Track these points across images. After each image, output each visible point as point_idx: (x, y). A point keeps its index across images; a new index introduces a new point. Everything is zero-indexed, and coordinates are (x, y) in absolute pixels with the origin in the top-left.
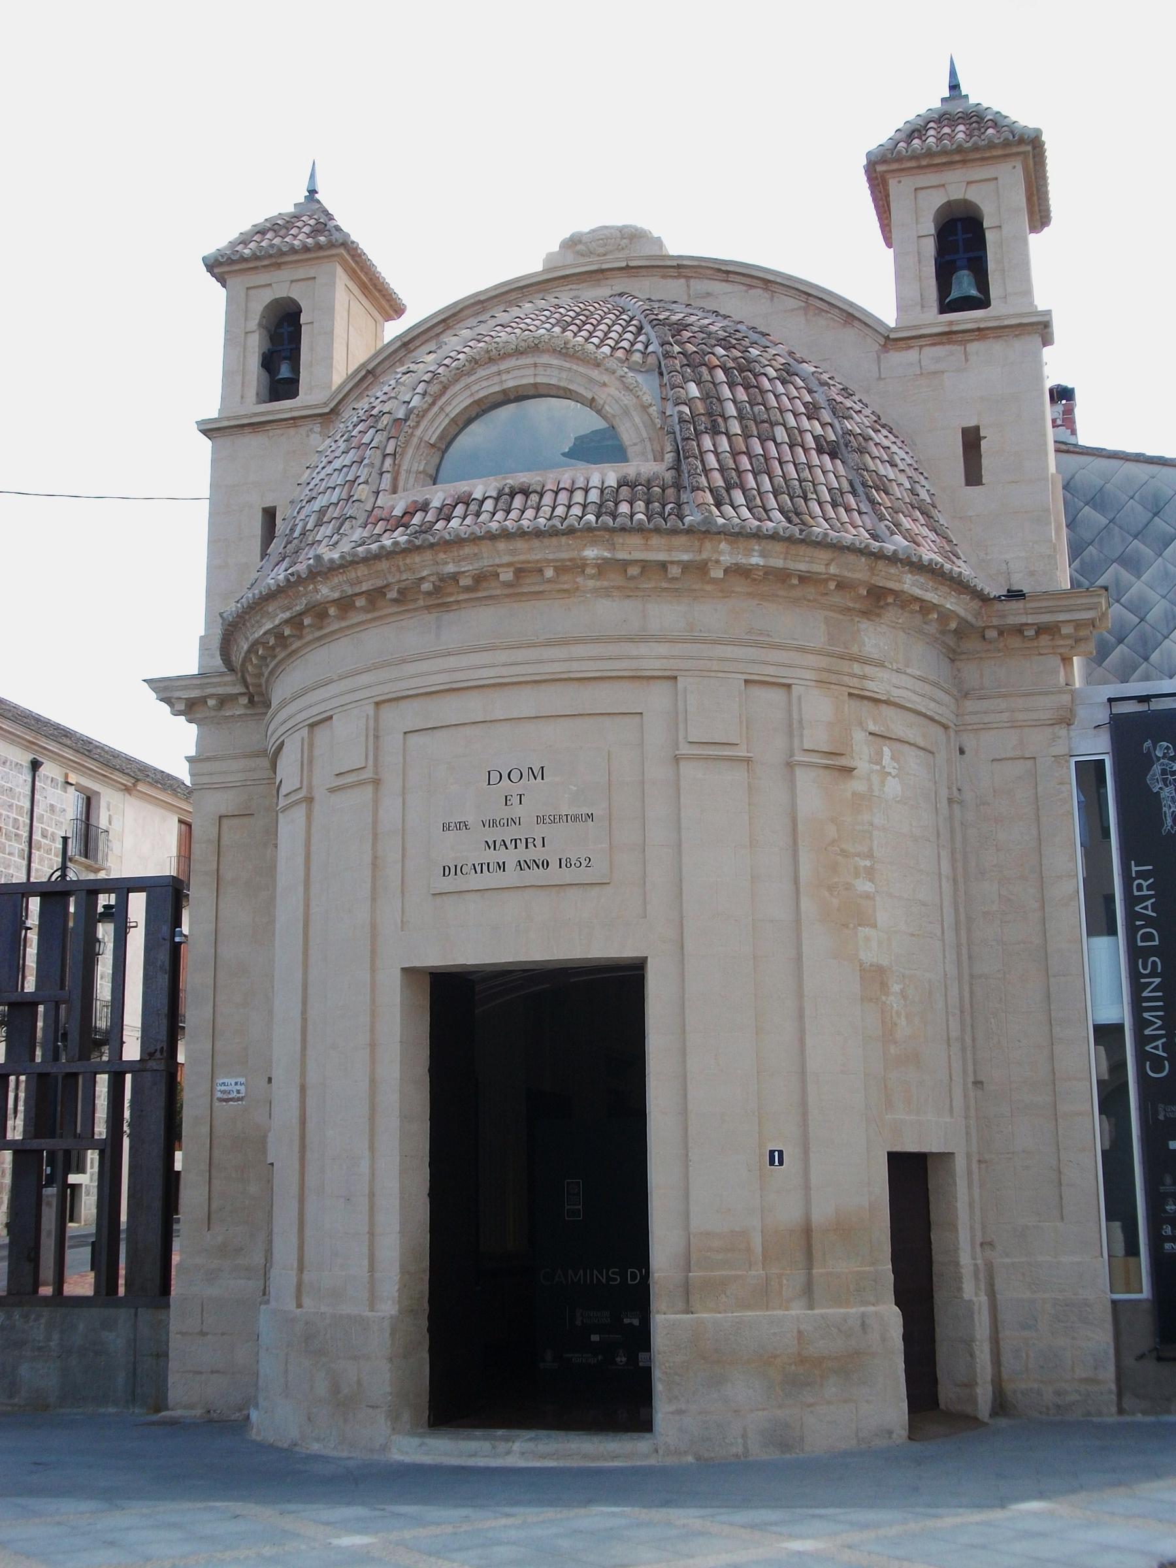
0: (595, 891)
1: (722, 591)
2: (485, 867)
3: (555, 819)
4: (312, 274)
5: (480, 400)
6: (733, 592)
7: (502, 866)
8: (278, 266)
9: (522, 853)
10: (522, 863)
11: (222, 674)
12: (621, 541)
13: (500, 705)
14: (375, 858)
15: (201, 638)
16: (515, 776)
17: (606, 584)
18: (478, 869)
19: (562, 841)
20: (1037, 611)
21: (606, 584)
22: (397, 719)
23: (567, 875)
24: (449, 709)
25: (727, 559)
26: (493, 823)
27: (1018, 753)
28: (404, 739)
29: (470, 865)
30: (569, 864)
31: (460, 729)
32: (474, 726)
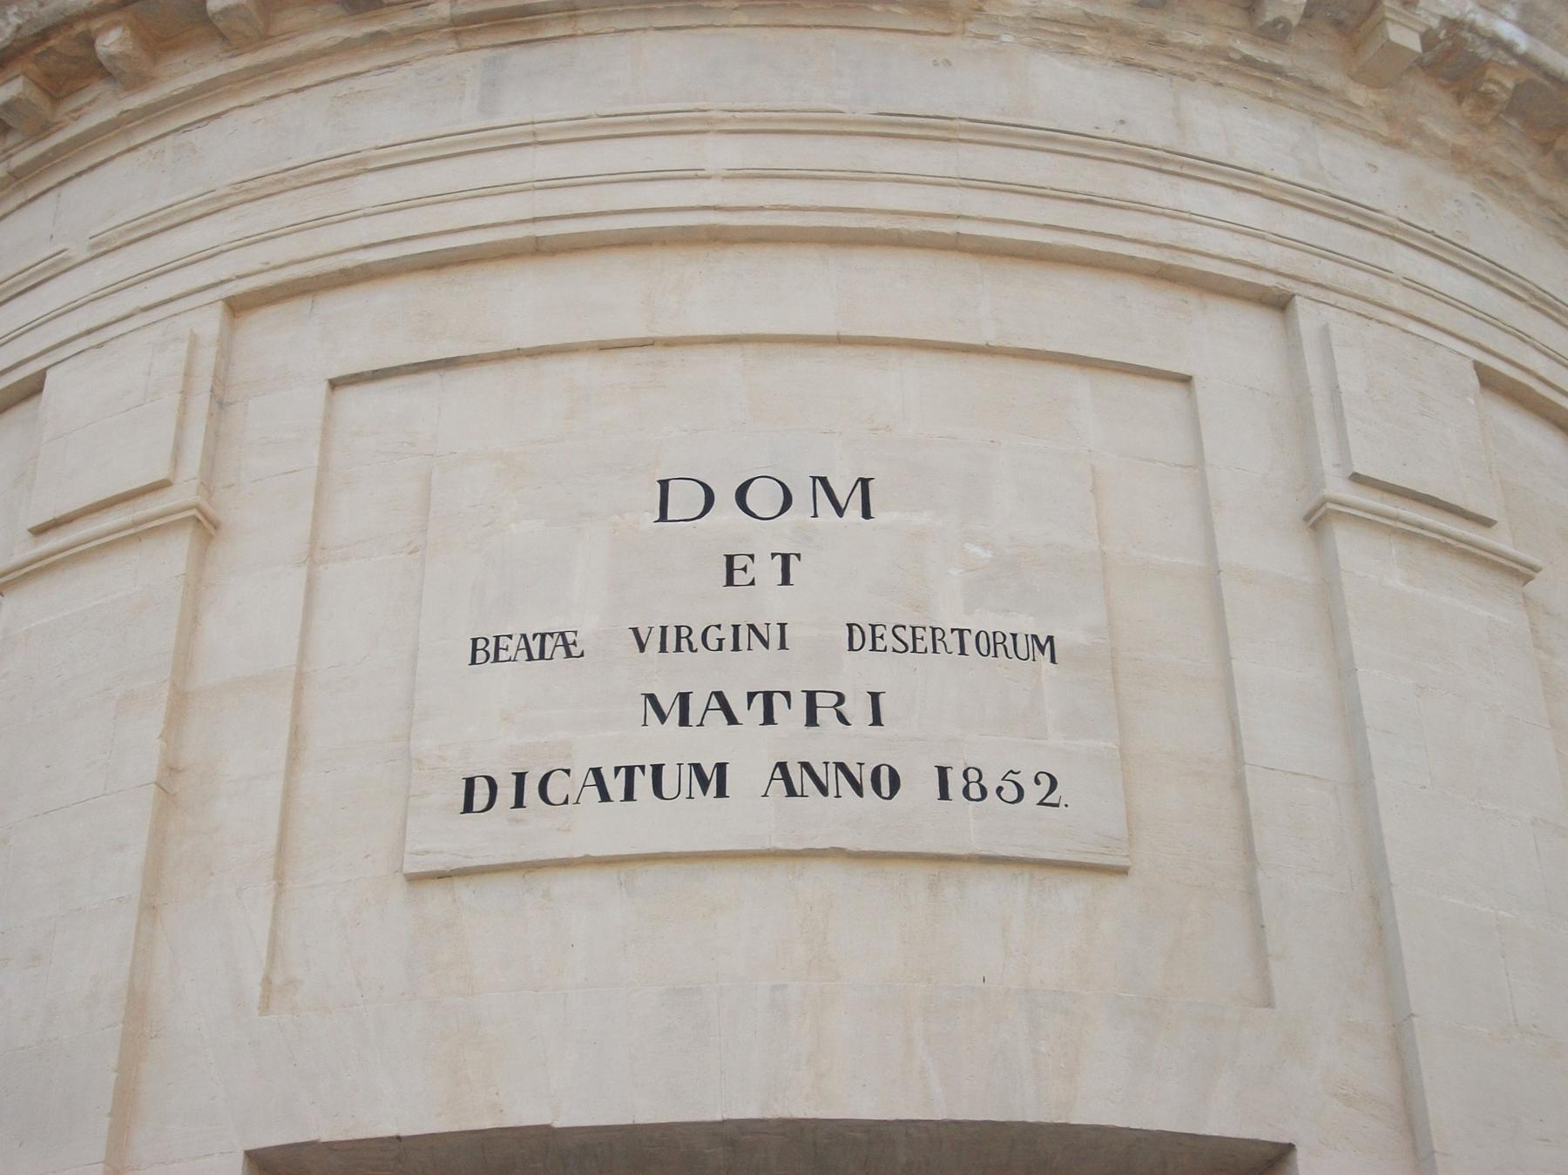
1: (1389, 118)
2: (643, 782)
6: (1418, 132)
7: (713, 780)
9: (790, 737)
10: (795, 772)
13: (705, 294)
14: (171, 769)
16: (763, 498)
18: (616, 786)
23: (967, 825)
24: (520, 304)
26: (677, 639)
28: (329, 401)
29: (580, 772)
30: (975, 789)
31: (551, 365)
32: (603, 358)
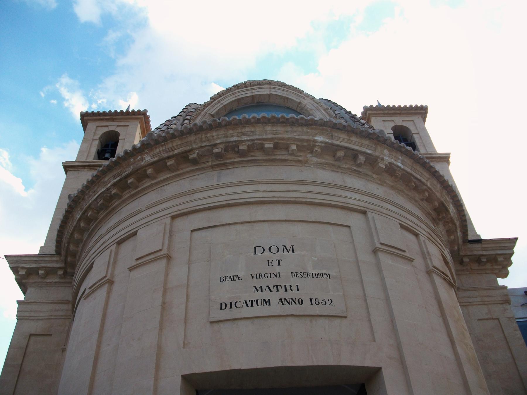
0: (337, 321)
3: (305, 275)
4: (127, 124)
5: (240, 99)
6: (385, 182)
7: (268, 302)
8: (113, 120)
9: (282, 293)
11: (52, 256)
12: (336, 135)
14: (164, 303)
15: (41, 247)
16: (274, 249)
17: (323, 161)
19: (309, 289)
20: (487, 249)
21: (323, 161)
22: (185, 225)
23: (317, 310)
25: (388, 159)
27: (489, 316)
29: (242, 301)
30: (317, 302)
31: (233, 227)
